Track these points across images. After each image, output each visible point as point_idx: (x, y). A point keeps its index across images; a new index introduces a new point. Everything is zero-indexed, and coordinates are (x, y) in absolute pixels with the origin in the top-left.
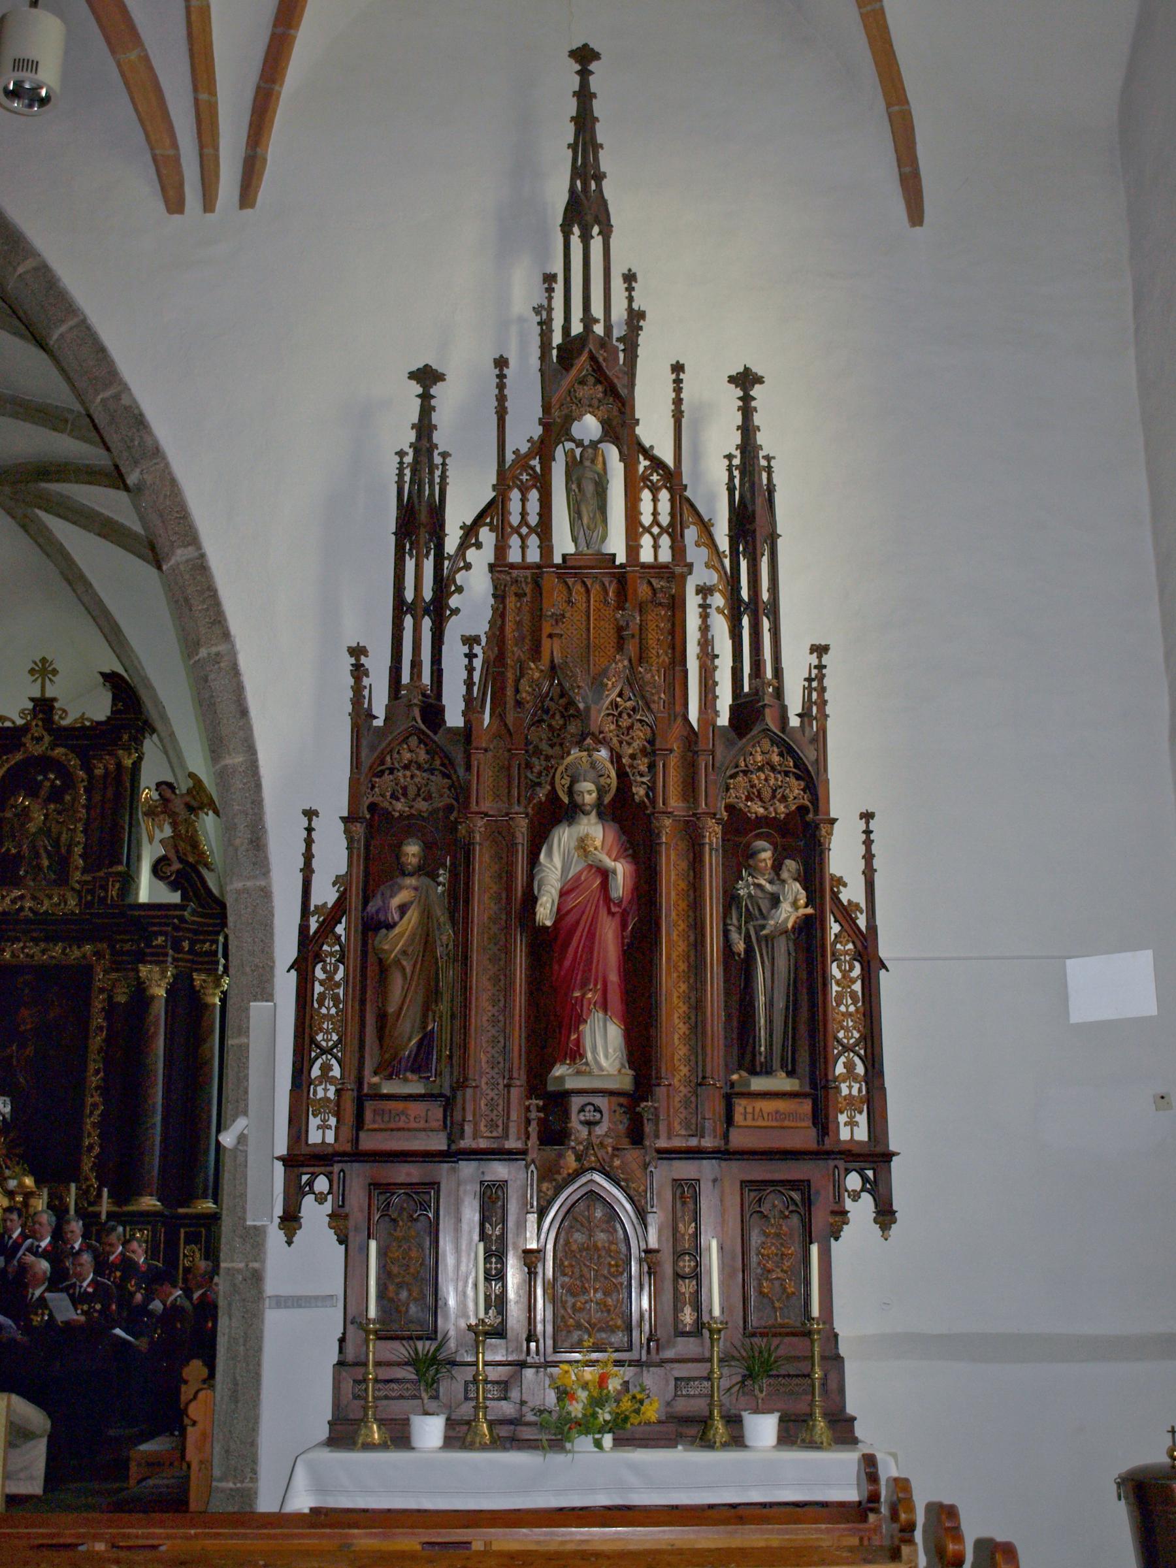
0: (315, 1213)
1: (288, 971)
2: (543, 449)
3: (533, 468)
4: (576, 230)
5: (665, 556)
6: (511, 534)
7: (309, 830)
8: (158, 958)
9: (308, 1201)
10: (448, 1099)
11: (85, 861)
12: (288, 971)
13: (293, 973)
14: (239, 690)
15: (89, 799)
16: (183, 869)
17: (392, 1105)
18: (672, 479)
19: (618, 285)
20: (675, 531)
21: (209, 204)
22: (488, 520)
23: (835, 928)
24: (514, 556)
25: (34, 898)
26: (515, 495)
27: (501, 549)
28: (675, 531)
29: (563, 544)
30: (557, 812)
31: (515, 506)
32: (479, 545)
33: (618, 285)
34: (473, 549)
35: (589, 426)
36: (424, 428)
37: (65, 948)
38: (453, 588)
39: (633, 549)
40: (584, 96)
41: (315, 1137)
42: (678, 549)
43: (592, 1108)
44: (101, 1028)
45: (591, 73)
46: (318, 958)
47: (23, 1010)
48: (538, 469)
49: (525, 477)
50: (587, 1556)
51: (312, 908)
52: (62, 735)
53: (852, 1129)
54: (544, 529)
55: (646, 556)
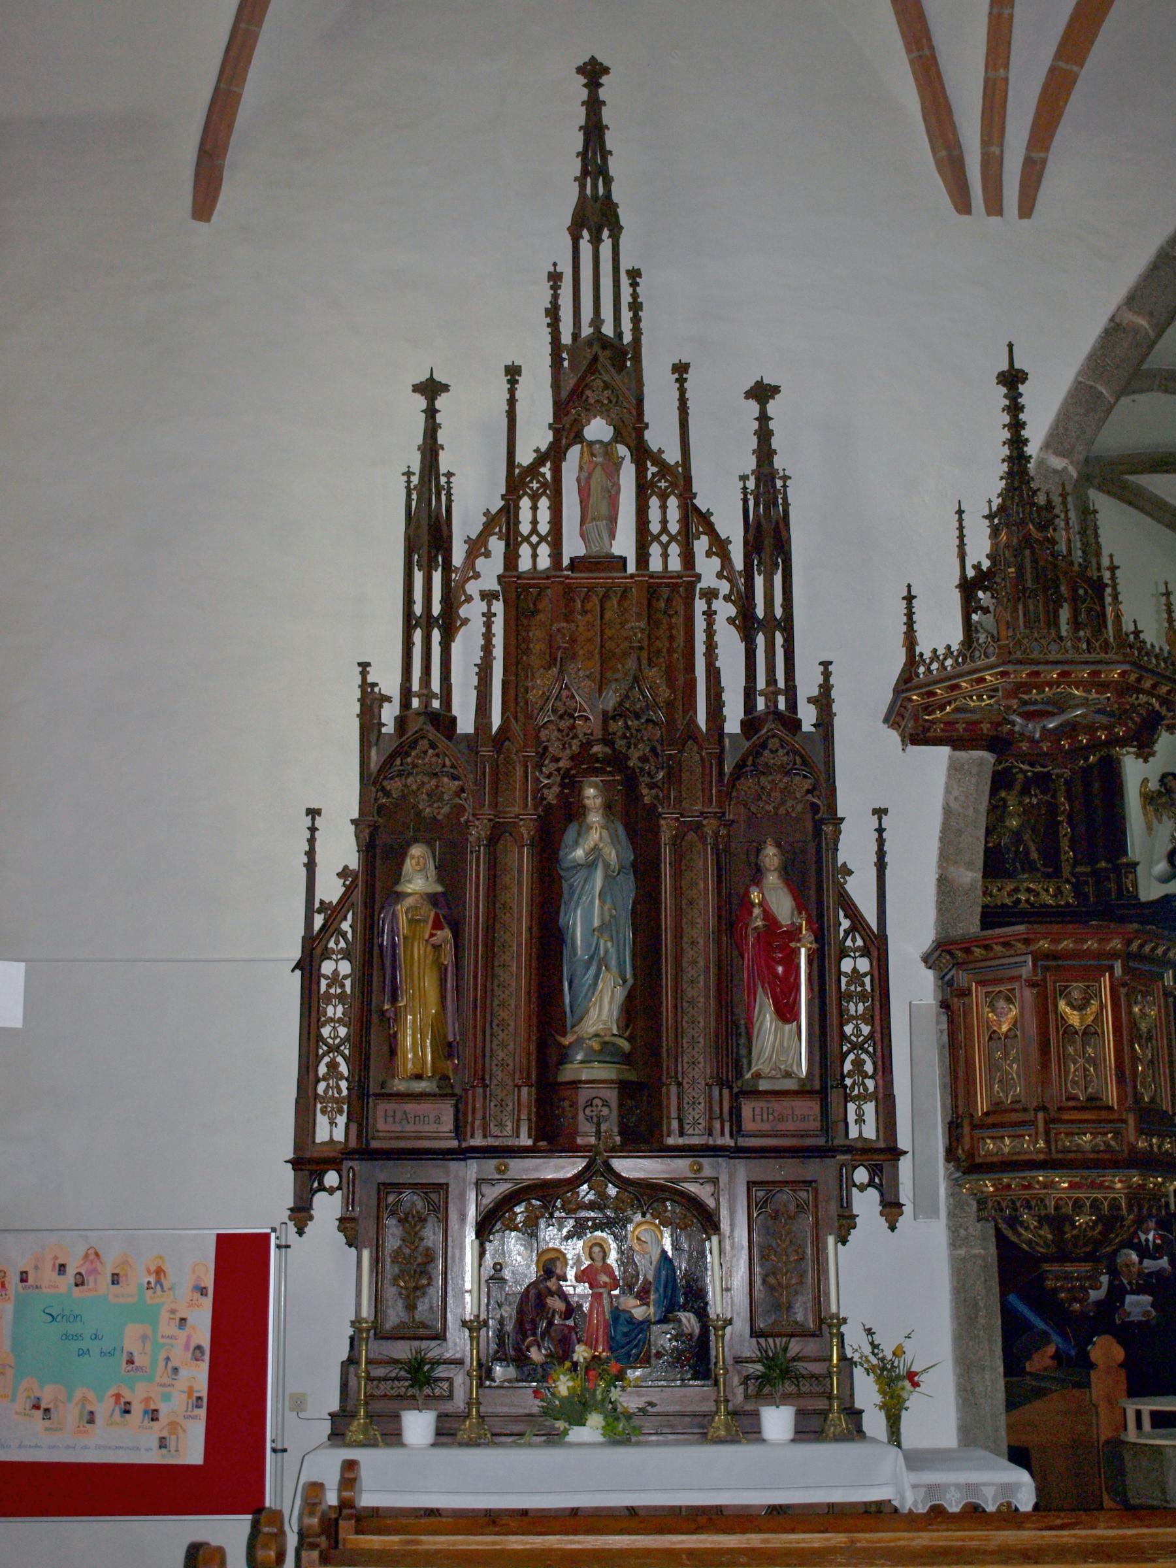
0: (327, 1208)
1: (293, 971)
2: (554, 454)
3: (543, 475)
4: (585, 234)
5: (675, 564)
6: (522, 542)
7: (313, 829)
9: (320, 1199)
10: (459, 1099)
12: (293, 971)
13: (298, 973)
17: (411, 1107)
18: (680, 480)
19: (625, 281)
20: (686, 540)
22: (497, 530)
23: (846, 924)
24: (525, 564)
26: (525, 503)
27: (511, 559)
28: (686, 540)
29: (573, 547)
31: (525, 514)
32: (488, 554)
33: (625, 281)
34: (482, 558)
35: (598, 429)
38: (463, 598)
39: (643, 558)
40: (594, 106)
41: (322, 1133)
42: (688, 558)
43: (600, 1103)
45: (601, 85)
46: (326, 955)
48: (548, 476)
49: (535, 485)
50: (574, 1557)
51: (317, 905)
53: (863, 1125)
54: (555, 538)
55: (655, 564)
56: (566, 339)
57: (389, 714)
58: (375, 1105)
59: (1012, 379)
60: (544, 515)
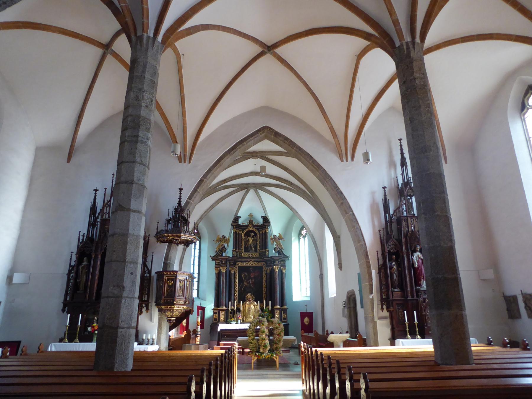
14: (362, 233)
16: (280, 252)
21: (347, 161)
24: (104, 217)
26: (105, 208)
27: (102, 216)
30: (415, 251)
36: (385, 195)
52: (254, 227)
56: (81, 241)
57: (85, 237)
58: (371, 389)
59: (181, 189)
60: (108, 210)
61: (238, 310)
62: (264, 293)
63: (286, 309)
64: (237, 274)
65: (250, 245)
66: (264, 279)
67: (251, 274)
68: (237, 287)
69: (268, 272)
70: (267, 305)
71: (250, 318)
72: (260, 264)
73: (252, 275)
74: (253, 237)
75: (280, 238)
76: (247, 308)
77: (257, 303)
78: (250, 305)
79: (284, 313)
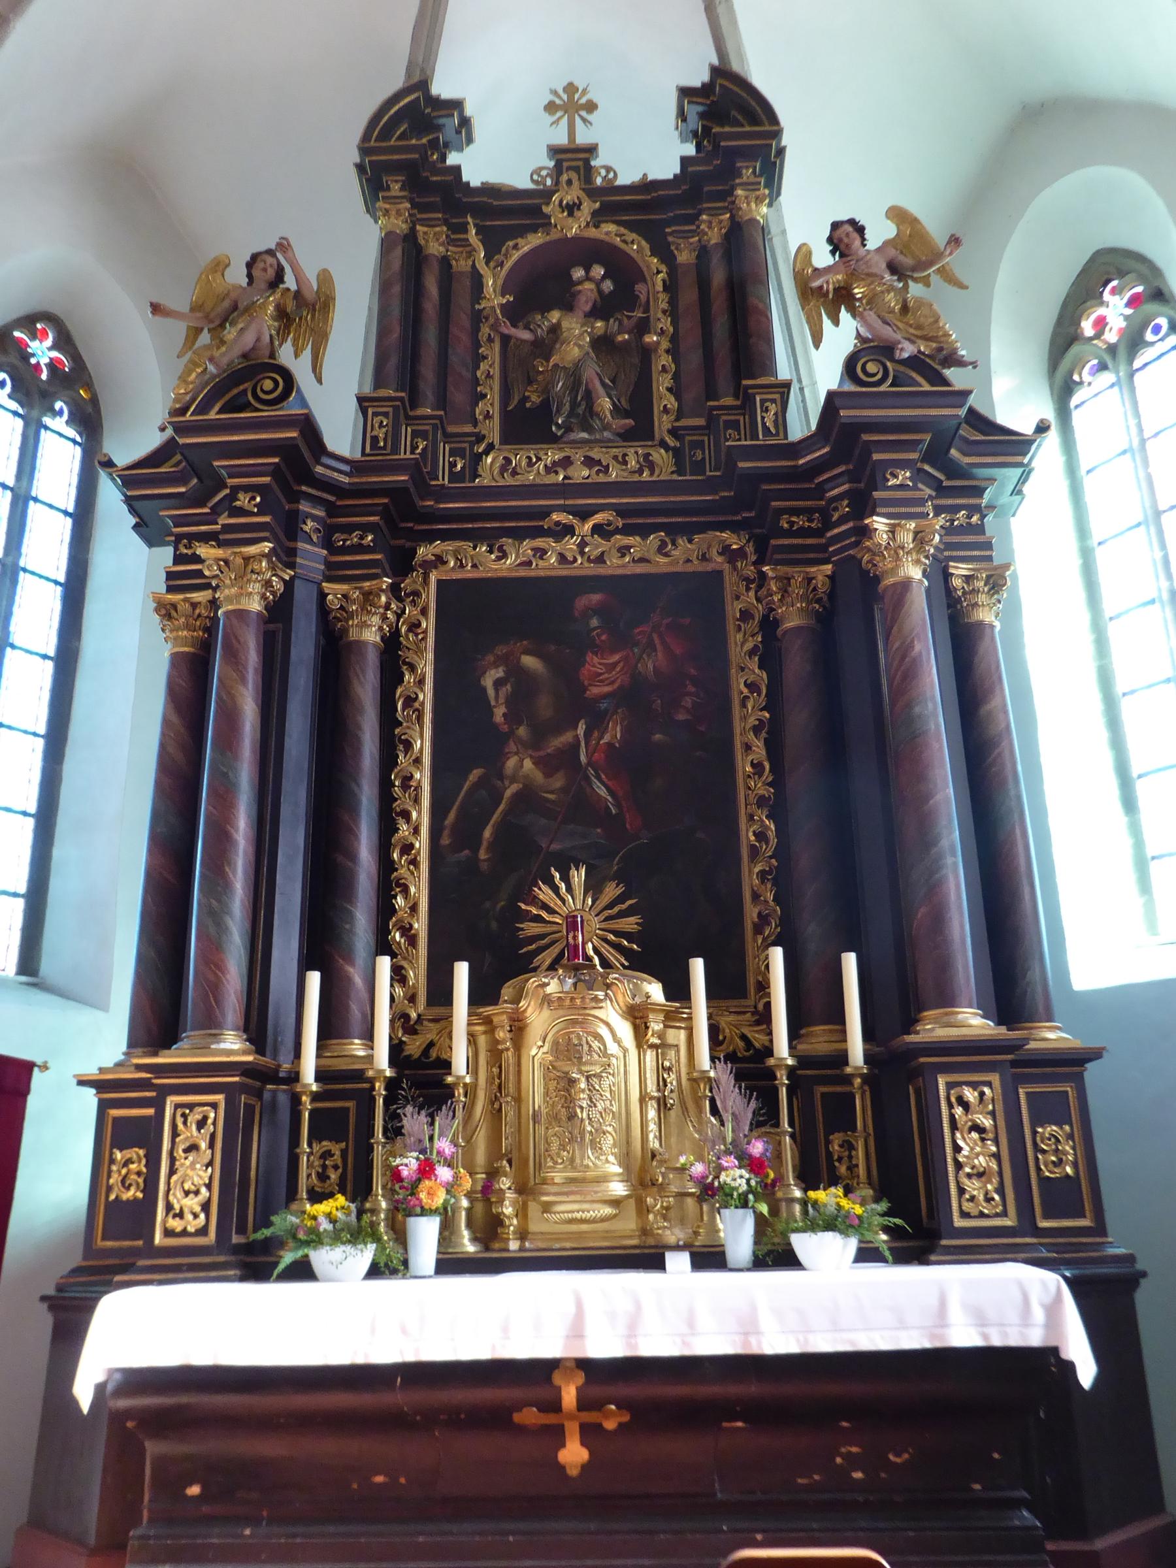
8: (903, 508)
11: (678, 398)
15: (673, 302)
25: (589, 462)
37: (663, 544)
44: (752, 687)
47: (590, 657)
61: (422, 1078)
62: (751, 875)
63: (1072, 1063)
64: (427, 665)
65: (574, 375)
66: (747, 716)
67: (594, 663)
68: (423, 815)
69: (793, 618)
70: (815, 1003)
71: (580, 1183)
72: (683, 555)
73: (602, 673)
74: (602, 309)
75: (913, 254)
76: (537, 1051)
77: (678, 990)
78: (576, 1013)
79: (1049, 1110)
